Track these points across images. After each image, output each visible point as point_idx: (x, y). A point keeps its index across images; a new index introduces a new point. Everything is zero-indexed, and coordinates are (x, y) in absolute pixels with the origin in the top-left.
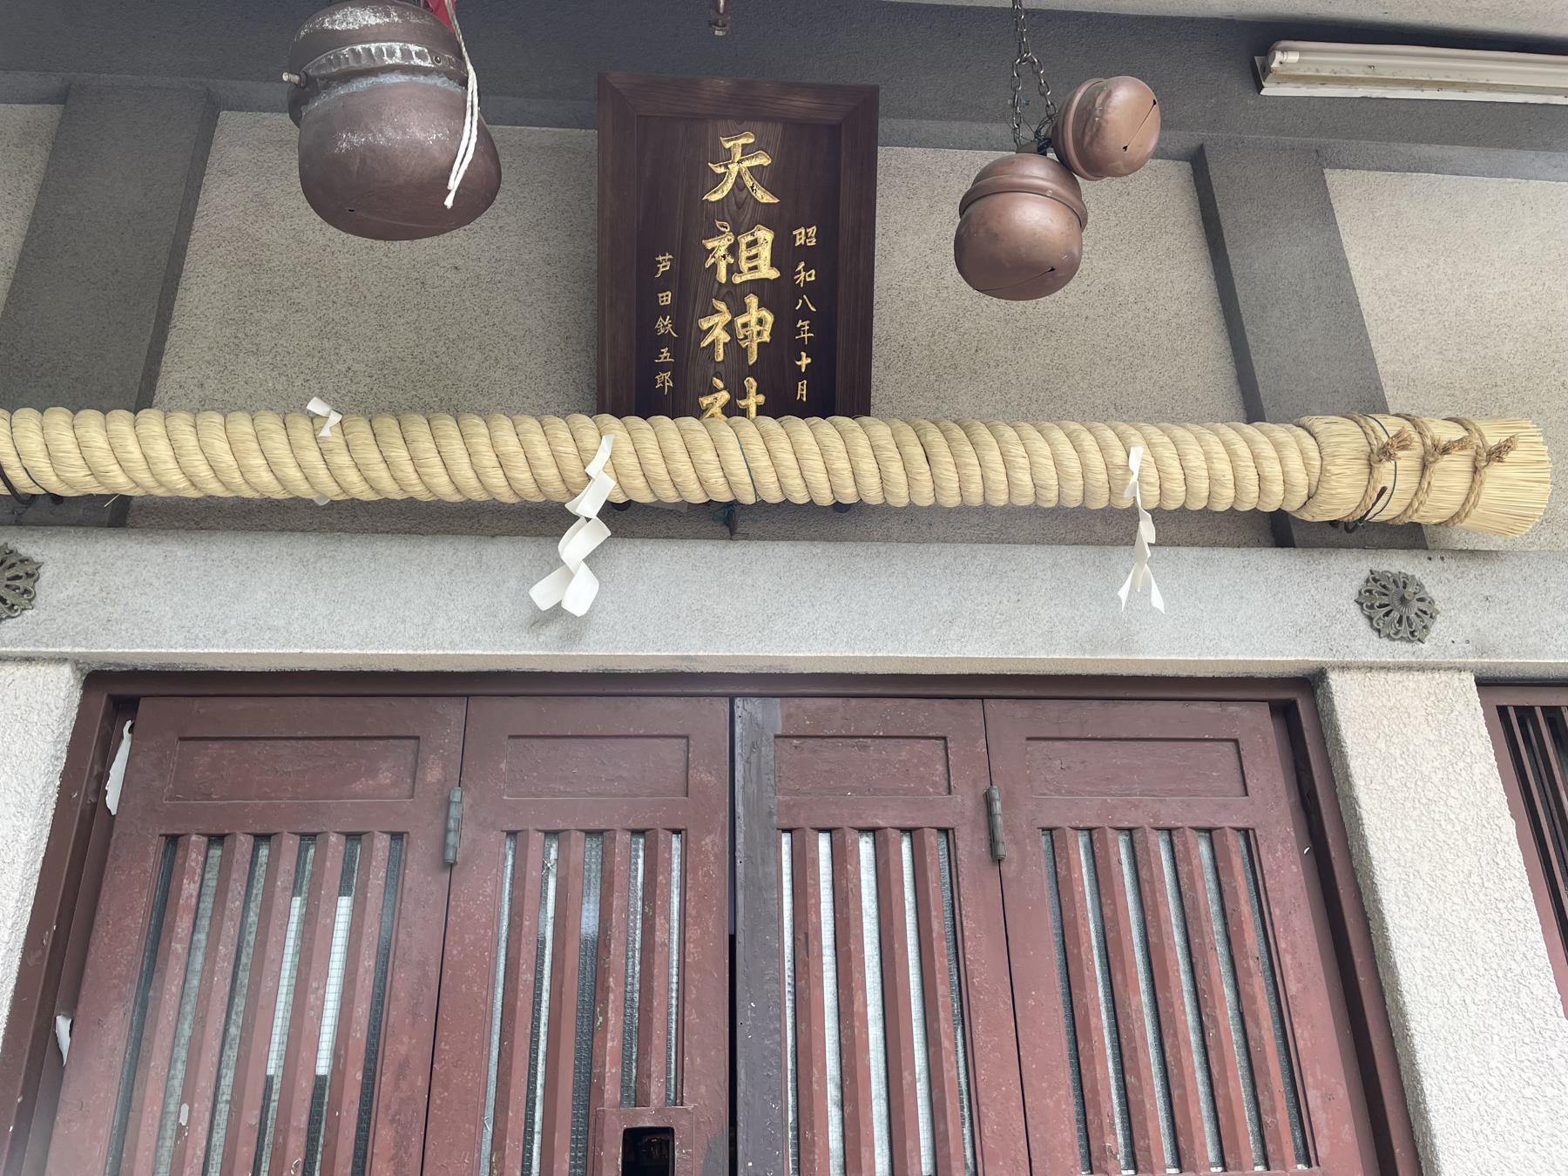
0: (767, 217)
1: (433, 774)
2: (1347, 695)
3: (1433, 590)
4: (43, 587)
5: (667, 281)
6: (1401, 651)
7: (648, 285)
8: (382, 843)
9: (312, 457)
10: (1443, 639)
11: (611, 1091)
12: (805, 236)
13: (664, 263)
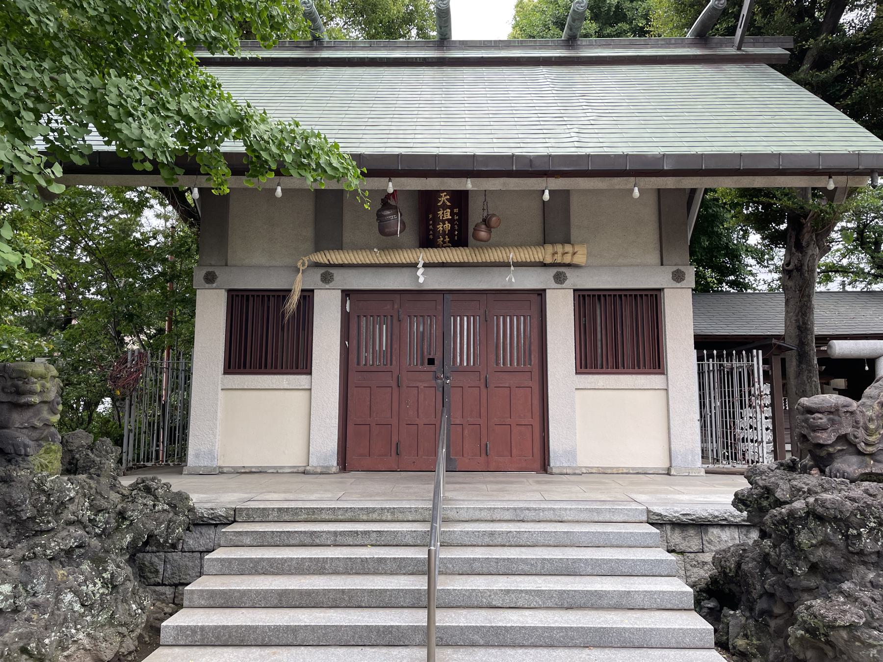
0: (449, 207)
1: (396, 306)
2: (549, 293)
3: (567, 275)
4: (334, 277)
5: (431, 219)
6: (559, 286)
7: (428, 220)
8: (389, 317)
9: (375, 258)
10: (567, 283)
11: (426, 353)
12: (456, 210)
13: (431, 216)
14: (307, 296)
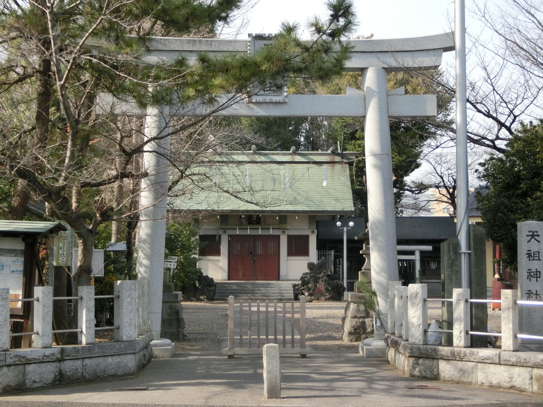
14: (220, 236)
